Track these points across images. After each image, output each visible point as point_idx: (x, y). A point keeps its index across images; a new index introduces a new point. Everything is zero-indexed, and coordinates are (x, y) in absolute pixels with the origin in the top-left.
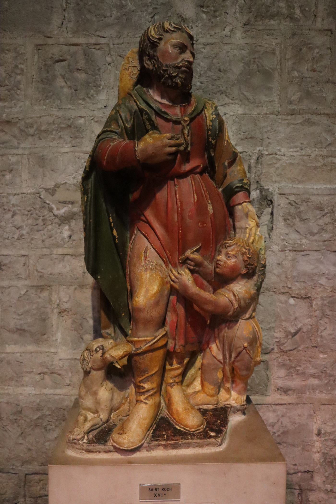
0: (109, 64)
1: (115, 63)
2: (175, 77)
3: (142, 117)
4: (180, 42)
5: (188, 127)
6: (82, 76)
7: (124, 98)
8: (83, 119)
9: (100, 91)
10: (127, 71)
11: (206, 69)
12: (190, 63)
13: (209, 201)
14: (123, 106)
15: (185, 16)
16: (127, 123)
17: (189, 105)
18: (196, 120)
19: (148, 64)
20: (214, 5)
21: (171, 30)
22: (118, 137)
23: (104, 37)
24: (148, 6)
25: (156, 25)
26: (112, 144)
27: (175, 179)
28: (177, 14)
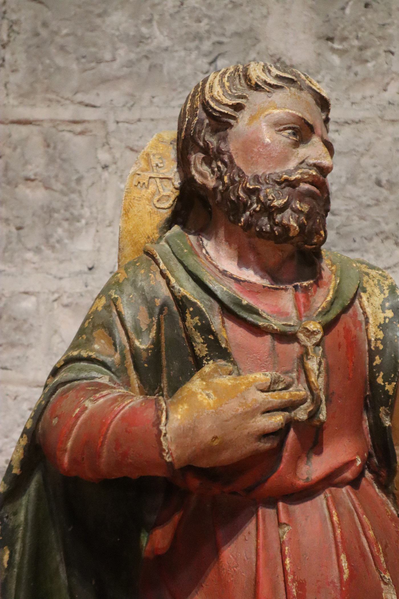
0: (105, 167)
1: (119, 164)
2: (281, 209)
3: (184, 320)
4: (293, 115)
5: (320, 350)
6: (35, 195)
7: (133, 263)
8: (33, 299)
9: (79, 231)
10: (144, 190)
11: (343, 180)
12: (324, 171)
13: (387, 577)
14: (128, 289)
15: (291, 60)
16: (138, 338)
17: (318, 286)
18: (339, 327)
19: (204, 174)
20: (360, 34)
21: (270, 85)
22: (111, 380)
23: (94, 106)
24: (201, 39)
25: (225, 73)
26: (88, 404)
27: (281, 504)
28: (272, 56)
